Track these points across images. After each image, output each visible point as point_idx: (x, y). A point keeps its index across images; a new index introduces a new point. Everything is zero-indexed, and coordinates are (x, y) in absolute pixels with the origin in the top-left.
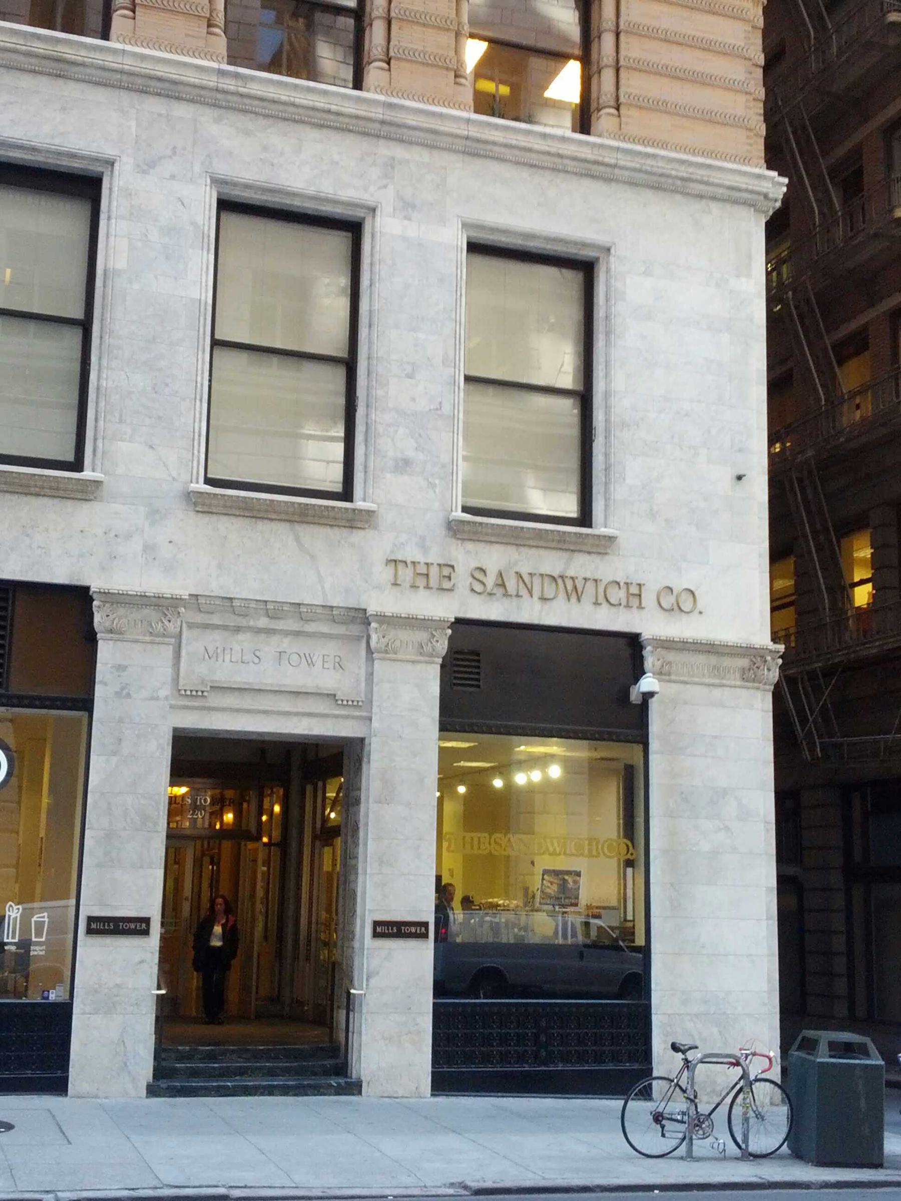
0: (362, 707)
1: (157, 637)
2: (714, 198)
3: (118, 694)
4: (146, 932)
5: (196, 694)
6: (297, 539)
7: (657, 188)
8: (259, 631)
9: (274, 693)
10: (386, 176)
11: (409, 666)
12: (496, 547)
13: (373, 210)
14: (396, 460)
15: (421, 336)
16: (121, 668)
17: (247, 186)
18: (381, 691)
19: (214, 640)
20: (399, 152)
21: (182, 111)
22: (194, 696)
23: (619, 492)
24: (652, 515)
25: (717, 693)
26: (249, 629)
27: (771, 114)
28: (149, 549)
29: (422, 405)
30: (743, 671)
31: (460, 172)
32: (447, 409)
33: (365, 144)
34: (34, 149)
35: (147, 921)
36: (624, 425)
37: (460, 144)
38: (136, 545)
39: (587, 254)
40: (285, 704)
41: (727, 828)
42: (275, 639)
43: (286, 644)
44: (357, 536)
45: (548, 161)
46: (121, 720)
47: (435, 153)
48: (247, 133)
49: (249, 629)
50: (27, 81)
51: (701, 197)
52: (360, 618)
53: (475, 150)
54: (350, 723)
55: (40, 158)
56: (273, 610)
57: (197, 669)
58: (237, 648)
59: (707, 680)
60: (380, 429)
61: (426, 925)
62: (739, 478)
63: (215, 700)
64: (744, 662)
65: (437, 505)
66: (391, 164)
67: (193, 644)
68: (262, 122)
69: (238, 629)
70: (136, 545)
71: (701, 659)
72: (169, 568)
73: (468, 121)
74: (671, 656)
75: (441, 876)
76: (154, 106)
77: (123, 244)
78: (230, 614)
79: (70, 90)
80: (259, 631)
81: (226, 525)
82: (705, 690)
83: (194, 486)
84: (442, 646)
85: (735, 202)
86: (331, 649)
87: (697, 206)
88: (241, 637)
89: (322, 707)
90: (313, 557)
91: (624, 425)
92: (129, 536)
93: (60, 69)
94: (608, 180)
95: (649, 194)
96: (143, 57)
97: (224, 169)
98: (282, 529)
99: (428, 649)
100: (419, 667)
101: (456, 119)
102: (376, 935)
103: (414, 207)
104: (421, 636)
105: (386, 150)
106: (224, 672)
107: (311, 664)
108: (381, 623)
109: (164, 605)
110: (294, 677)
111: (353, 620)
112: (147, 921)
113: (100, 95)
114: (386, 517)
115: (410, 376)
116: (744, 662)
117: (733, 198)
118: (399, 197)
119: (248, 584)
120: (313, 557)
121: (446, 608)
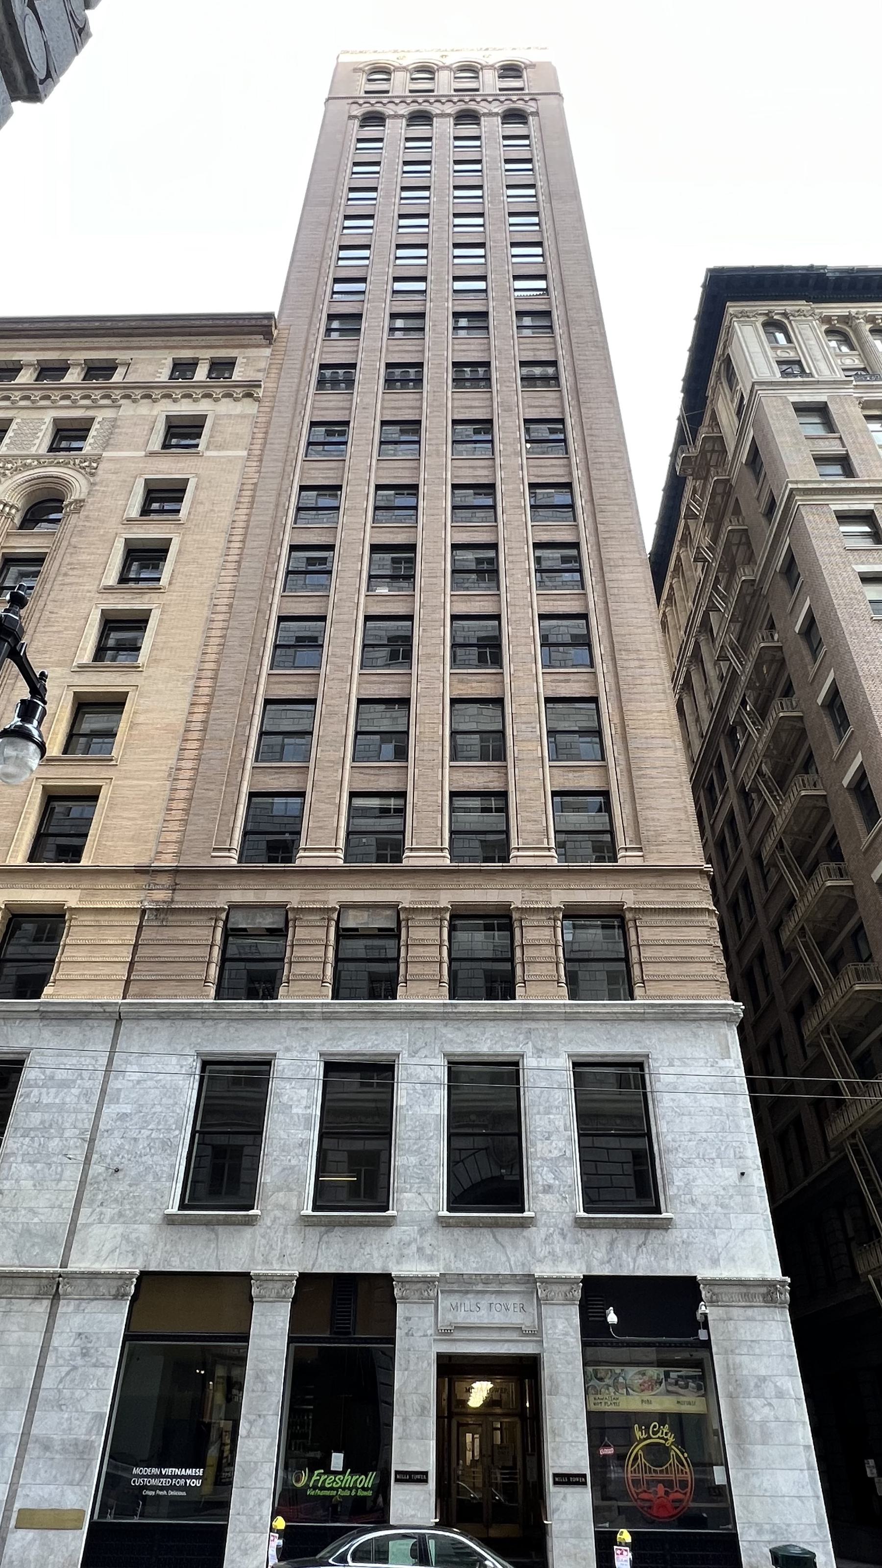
0: (537, 1333)
1: (425, 1301)
2: (702, 1020)
3: (407, 1334)
4: (426, 1481)
5: (447, 1332)
6: (494, 1237)
7: (670, 1020)
8: (478, 1292)
9: (490, 1326)
10: (527, 1038)
11: (561, 1307)
12: (604, 1231)
13: (523, 1056)
14: (543, 1186)
15: (552, 1117)
16: (408, 1319)
17: (461, 1055)
18: (547, 1322)
19: (454, 1299)
20: (533, 1025)
21: (428, 1024)
22: (445, 1333)
23: (672, 1191)
24: (693, 1202)
25: (750, 1312)
26: (472, 1292)
27: (729, 971)
28: (420, 1249)
29: (556, 1153)
30: (764, 1296)
31: (565, 1031)
32: (568, 1154)
33: (516, 1025)
34: (364, 1055)
35: (426, 1473)
36: (669, 1151)
37: (621, 1017)
38: (414, 1248)
39: (639, 1059)
40: (495, 1336)
41: (770, 1404)
42: (487, 1296)
43: (493, 1299)
44: (526, 1233)
45: (608, 1017)
46: (409, 1350)
47: (551, 1023)
48: (459, 1029)
49: (472, 1292)
50: (361, 1024)
51: (695, 1020)
52: (530, 1279)
53: (570, 1018)
54: (531, 1345)
55: (367, 1058)
56: (487, 1279)
57: (447, 1317)
58: (467, 1302)
59: (743, 1304)
60: (534, 1169)
61: (584, 1476)
62: (743, 1174)
63: (457, 1335)
64: (764, 1290)
65: (568, 1209)
66: (529, 1031)
67: (444, 1302)
68: (466, 1023)
69: (467, 1292)
70: (414, 1248)
71: (735, 1290)
72: (430, 1259)
73: (564, 1005)
74: (716, 1290)
75: (767, 1149)
76: (417, 1024)
77: (404, 1093)
78: (460, 1284)
79: (380, 1024)
80: (478, 1292)
81: (459, 1233)
82: (743, 1310)
83: (441, 1214)
84: (578, 1294)
85: (715, 1020)
86: (516, 1300)
87: (693, 1025)
88: (469, 1296)
89: (515, 1336)
90: (503, 1247)
91: (669, 1151)
92: (409, 1244)
93: (375, 1016)
94: (643, 1020)
95: (666, 1023)
96: (410, 1004)
97: (449, 1049)
98: (485, 1231)
99: (570, 1296)
100: (566, 1307)
101: (559, 1005)
102: (555, 1483)
103: (543, 1051)
104: (566, 1288)
105: (526, 1025)
106: (462, 1317)
107: (507, 1309)
108: (542, 1283)
109: (427, 1281)
110: (498, 1318)
111: (528, 1282)
112: (426, 1473)
113: (392, 1024)
114: (543, 1219)
115: (547, 1139)
116: (764, 1290)
117: (714, 1017)
118: (534, 1047)
119: (470, 1266)
120: (503, 1247)
121: (577, 1271)
